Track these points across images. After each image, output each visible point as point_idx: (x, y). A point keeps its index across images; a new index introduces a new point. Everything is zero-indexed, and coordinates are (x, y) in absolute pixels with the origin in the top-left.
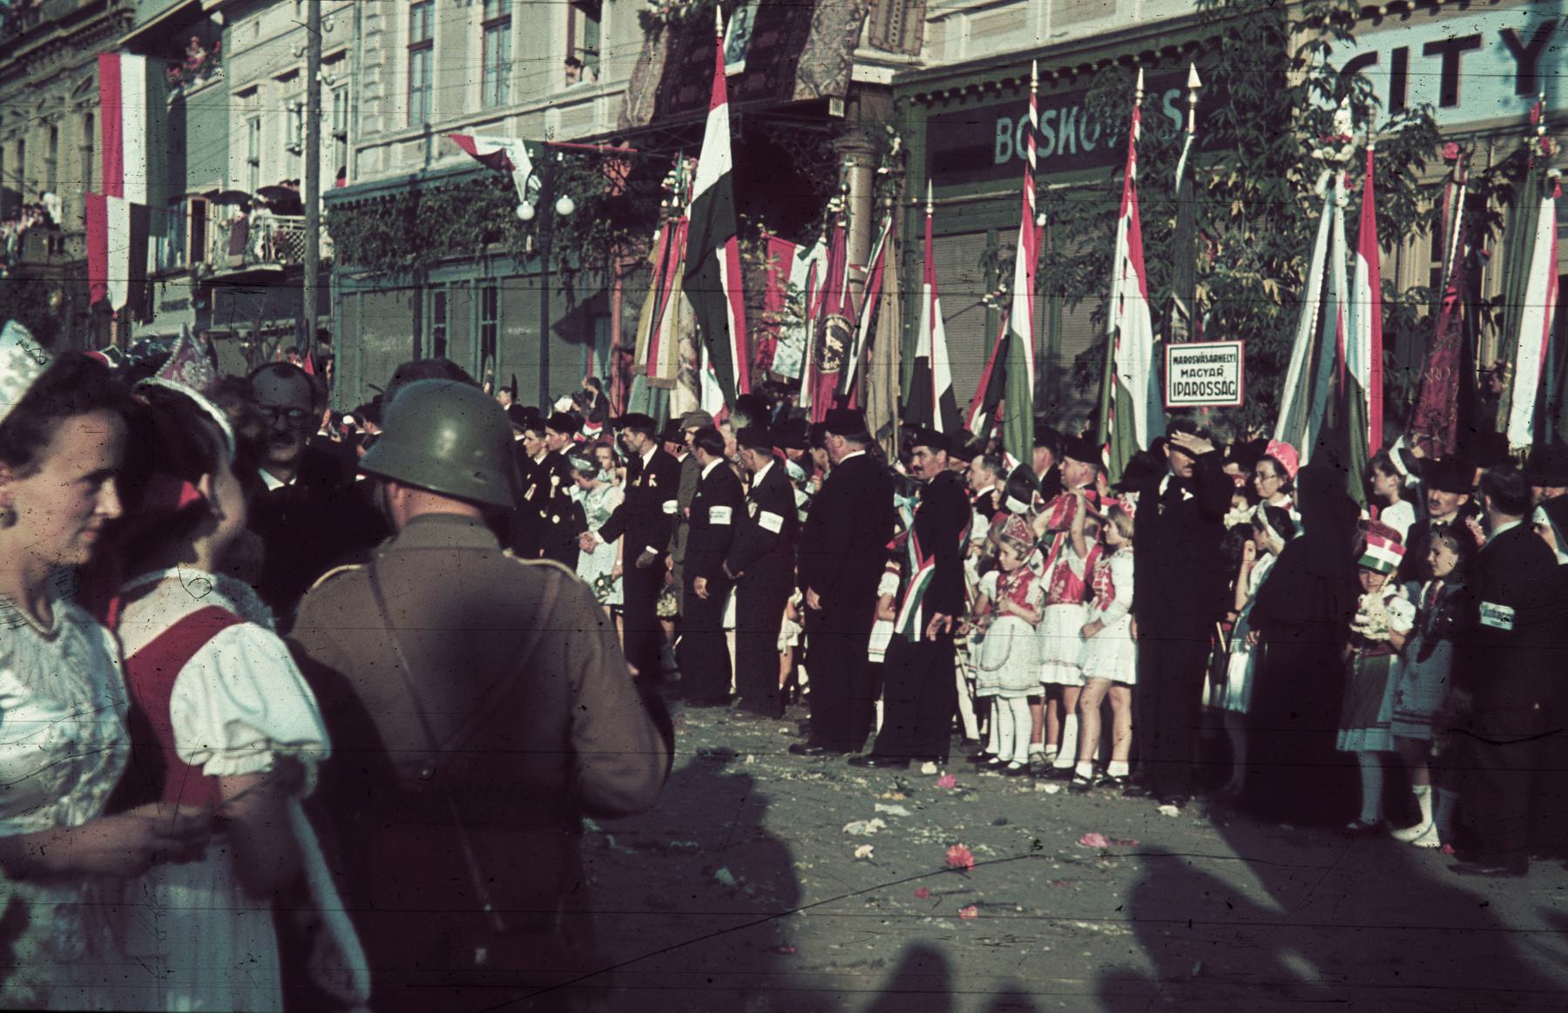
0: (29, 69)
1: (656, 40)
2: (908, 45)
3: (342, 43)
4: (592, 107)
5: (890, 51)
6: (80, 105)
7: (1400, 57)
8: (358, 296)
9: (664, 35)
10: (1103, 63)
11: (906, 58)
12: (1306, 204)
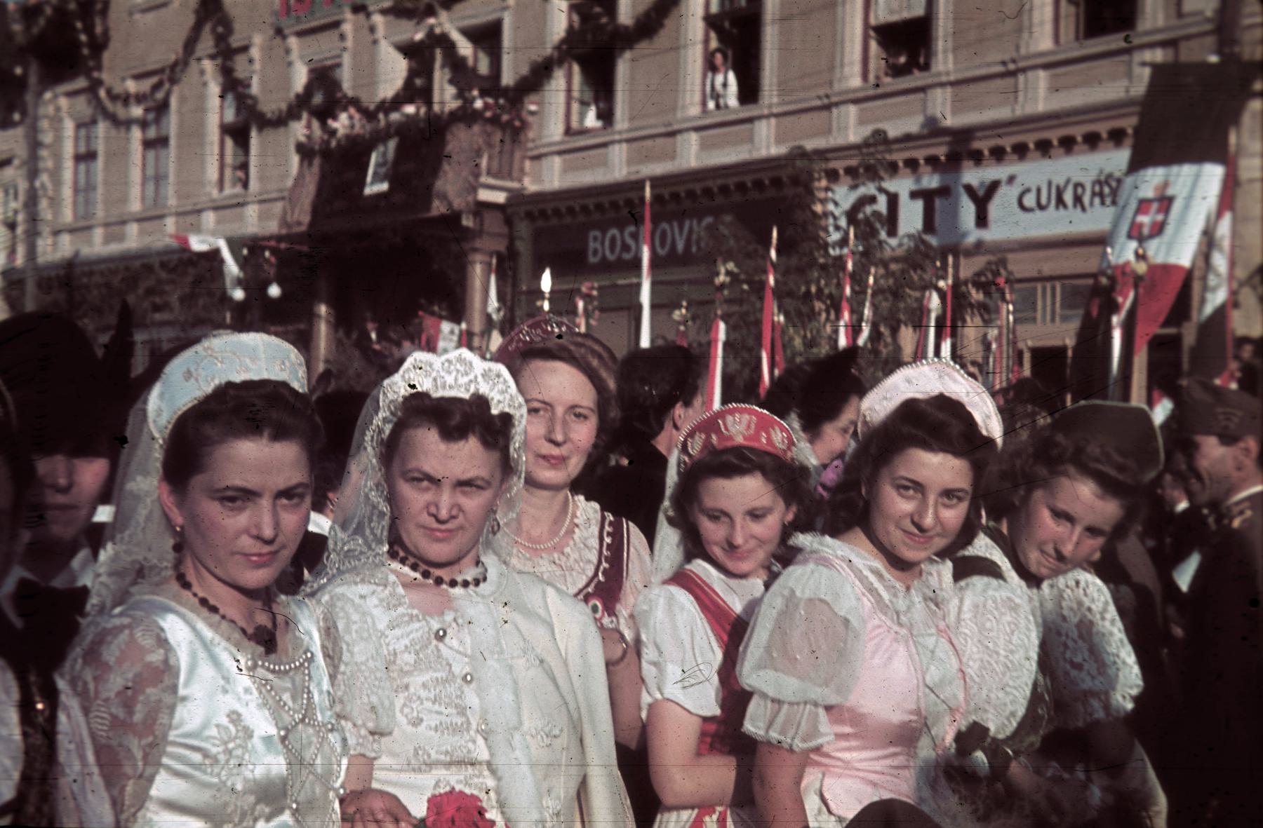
1: (310, 164)
2: (515, 174)
5: (502, 178)
7: (893, 200)
9: (317, 162)
11: (515, 185)
12: (818, 305)
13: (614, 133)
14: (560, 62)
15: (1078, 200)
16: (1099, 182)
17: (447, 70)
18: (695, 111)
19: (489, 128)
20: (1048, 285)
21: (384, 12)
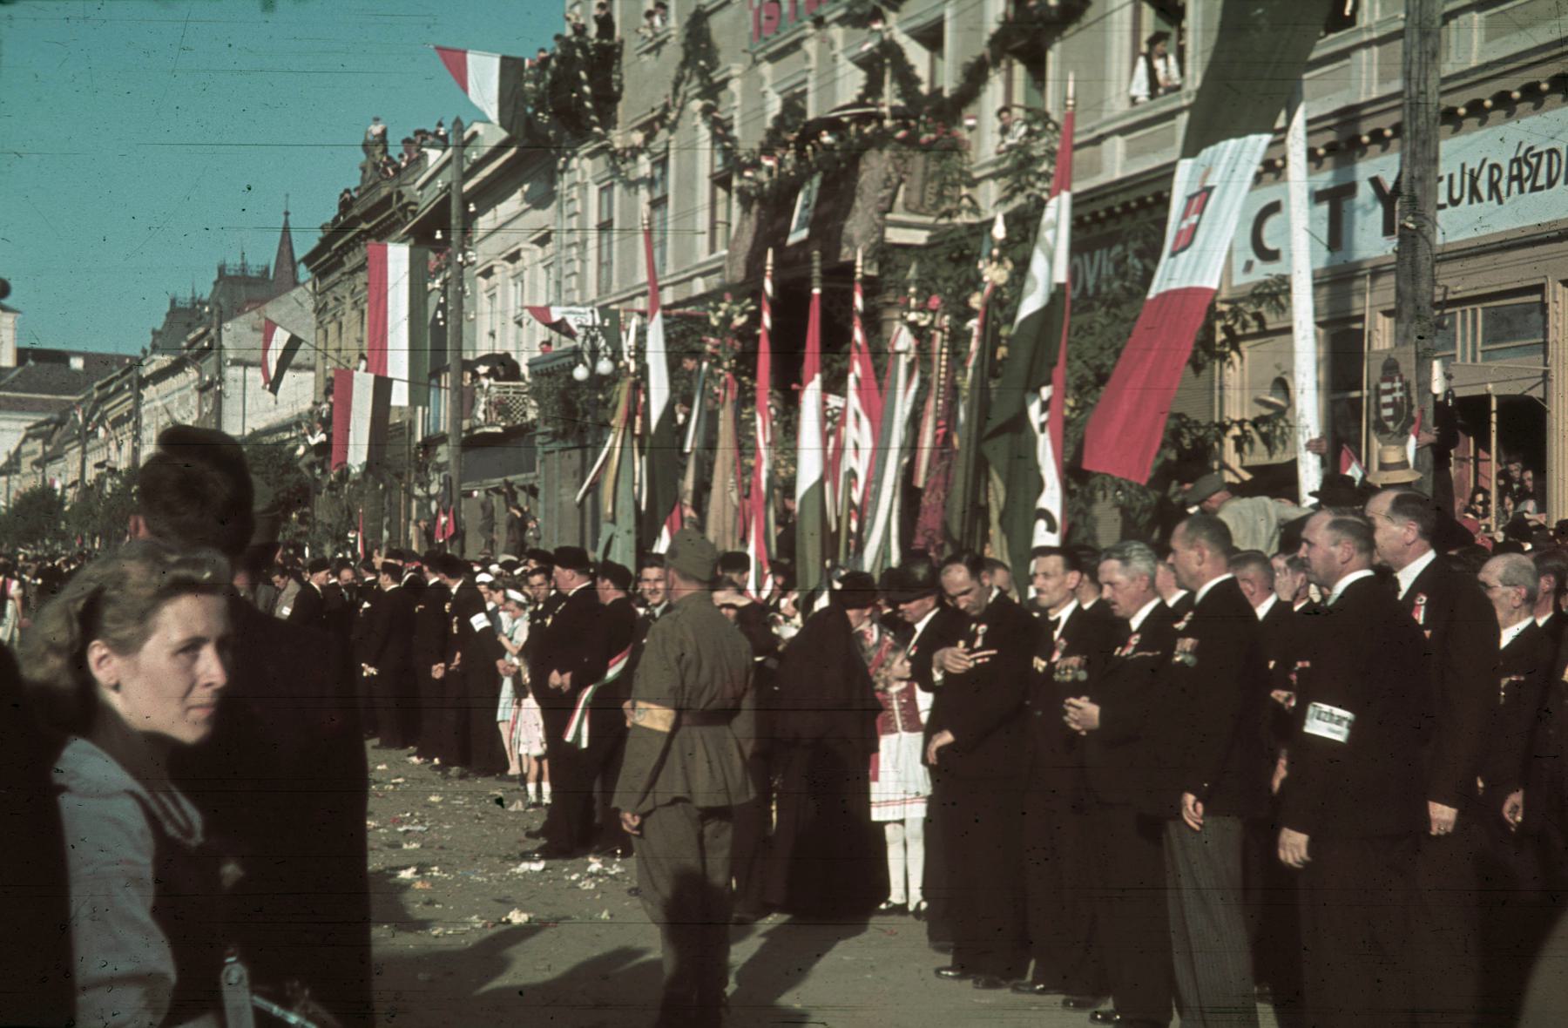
0: (345, 259)
3: (517, 244)
4: (1173, 126)
6: (356, 302)
8: (556, 454)
9: (755, 208)
10: (1125, 206)
13: (1360, 31)
14: (996, 63)
15: (1494, 186)
16: (1516, 160)
17: (895, 86)
18: (1122, 106)
19: (905, 151)
20: (1468, 308)
21: (841, 21)
